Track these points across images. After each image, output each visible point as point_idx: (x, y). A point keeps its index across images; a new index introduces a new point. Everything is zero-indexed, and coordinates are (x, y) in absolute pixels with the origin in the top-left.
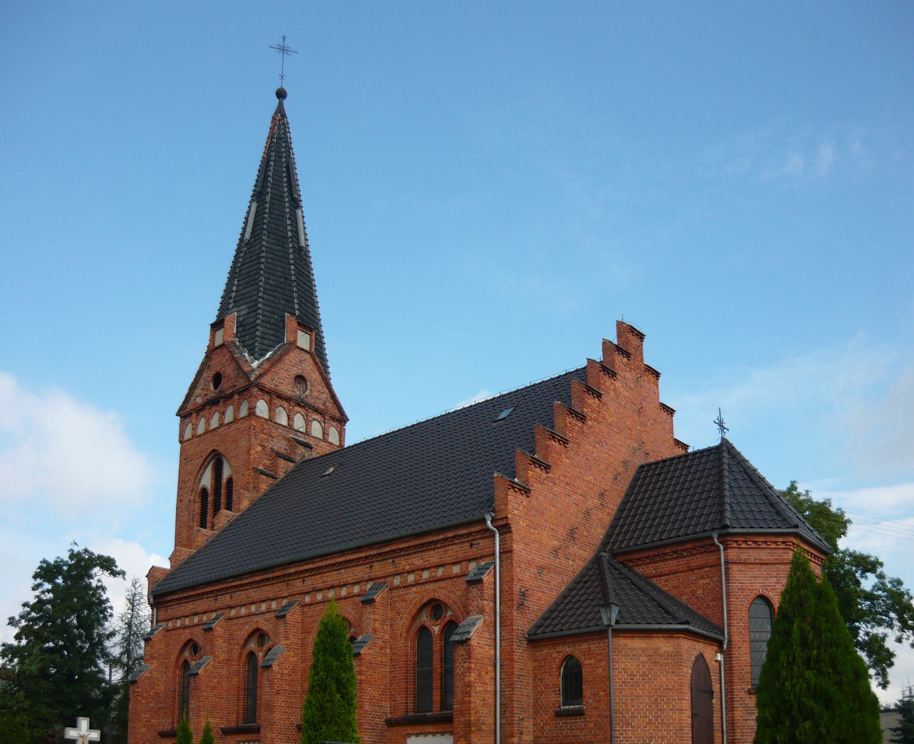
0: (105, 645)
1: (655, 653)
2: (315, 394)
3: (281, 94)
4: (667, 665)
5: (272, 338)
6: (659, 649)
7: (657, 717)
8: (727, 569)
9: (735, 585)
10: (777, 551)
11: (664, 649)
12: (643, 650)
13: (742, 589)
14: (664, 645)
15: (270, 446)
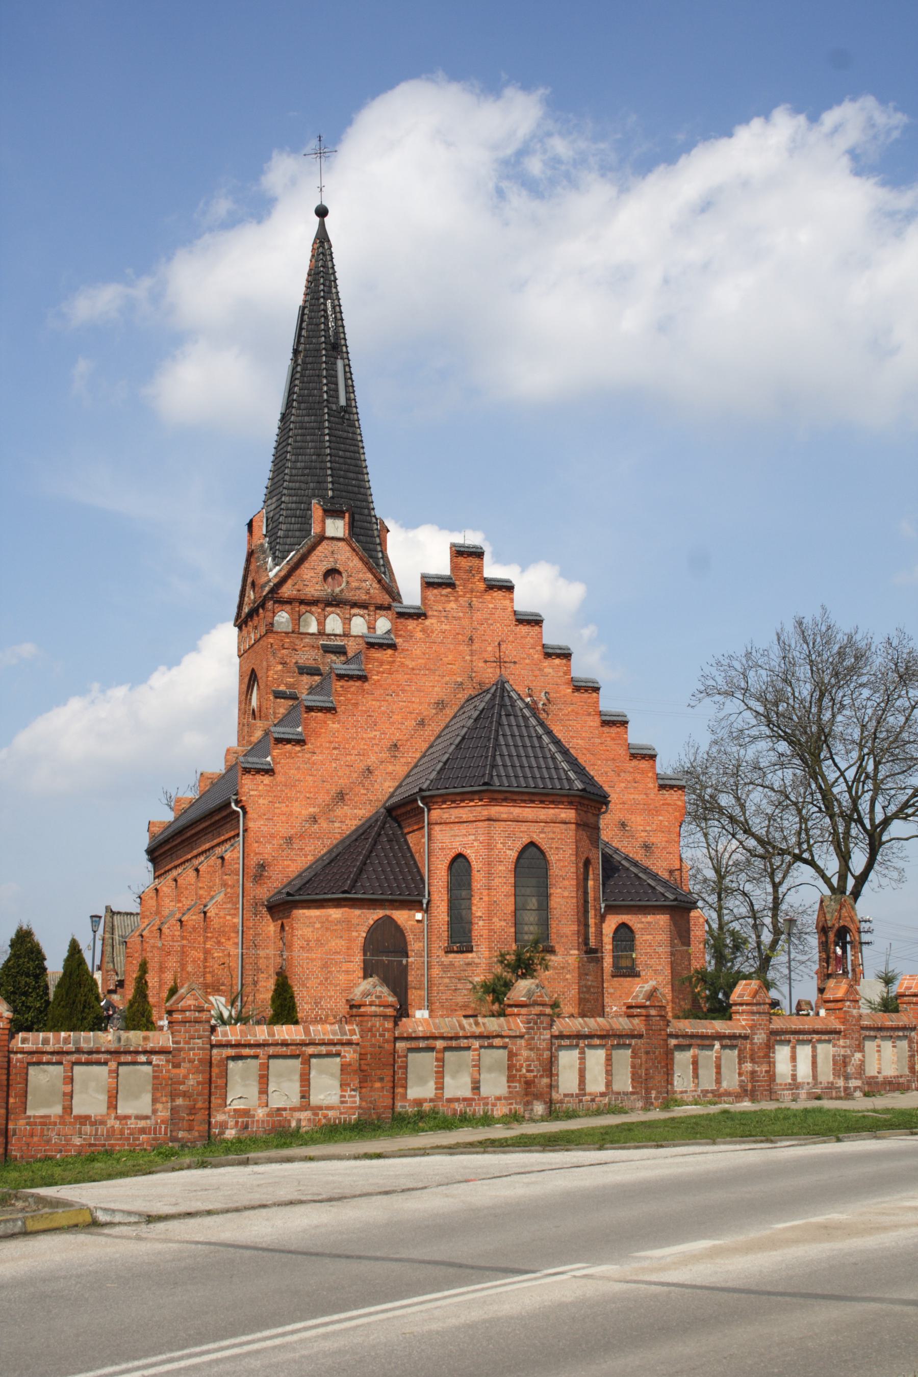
0: (573, 811)
1: (327, 920)
2: (354, 584)
3: (322, 212)
4: (336, 930)
5: (297, 534)
6: (330, 916)
7: (326, 979)
8: (429, 830)
9: (436, 845)
10: (477, 808)
11: (334, 916)
12: (317, 917)
13: (442, 849)
14: (335, 913)
15: (294, 661)
